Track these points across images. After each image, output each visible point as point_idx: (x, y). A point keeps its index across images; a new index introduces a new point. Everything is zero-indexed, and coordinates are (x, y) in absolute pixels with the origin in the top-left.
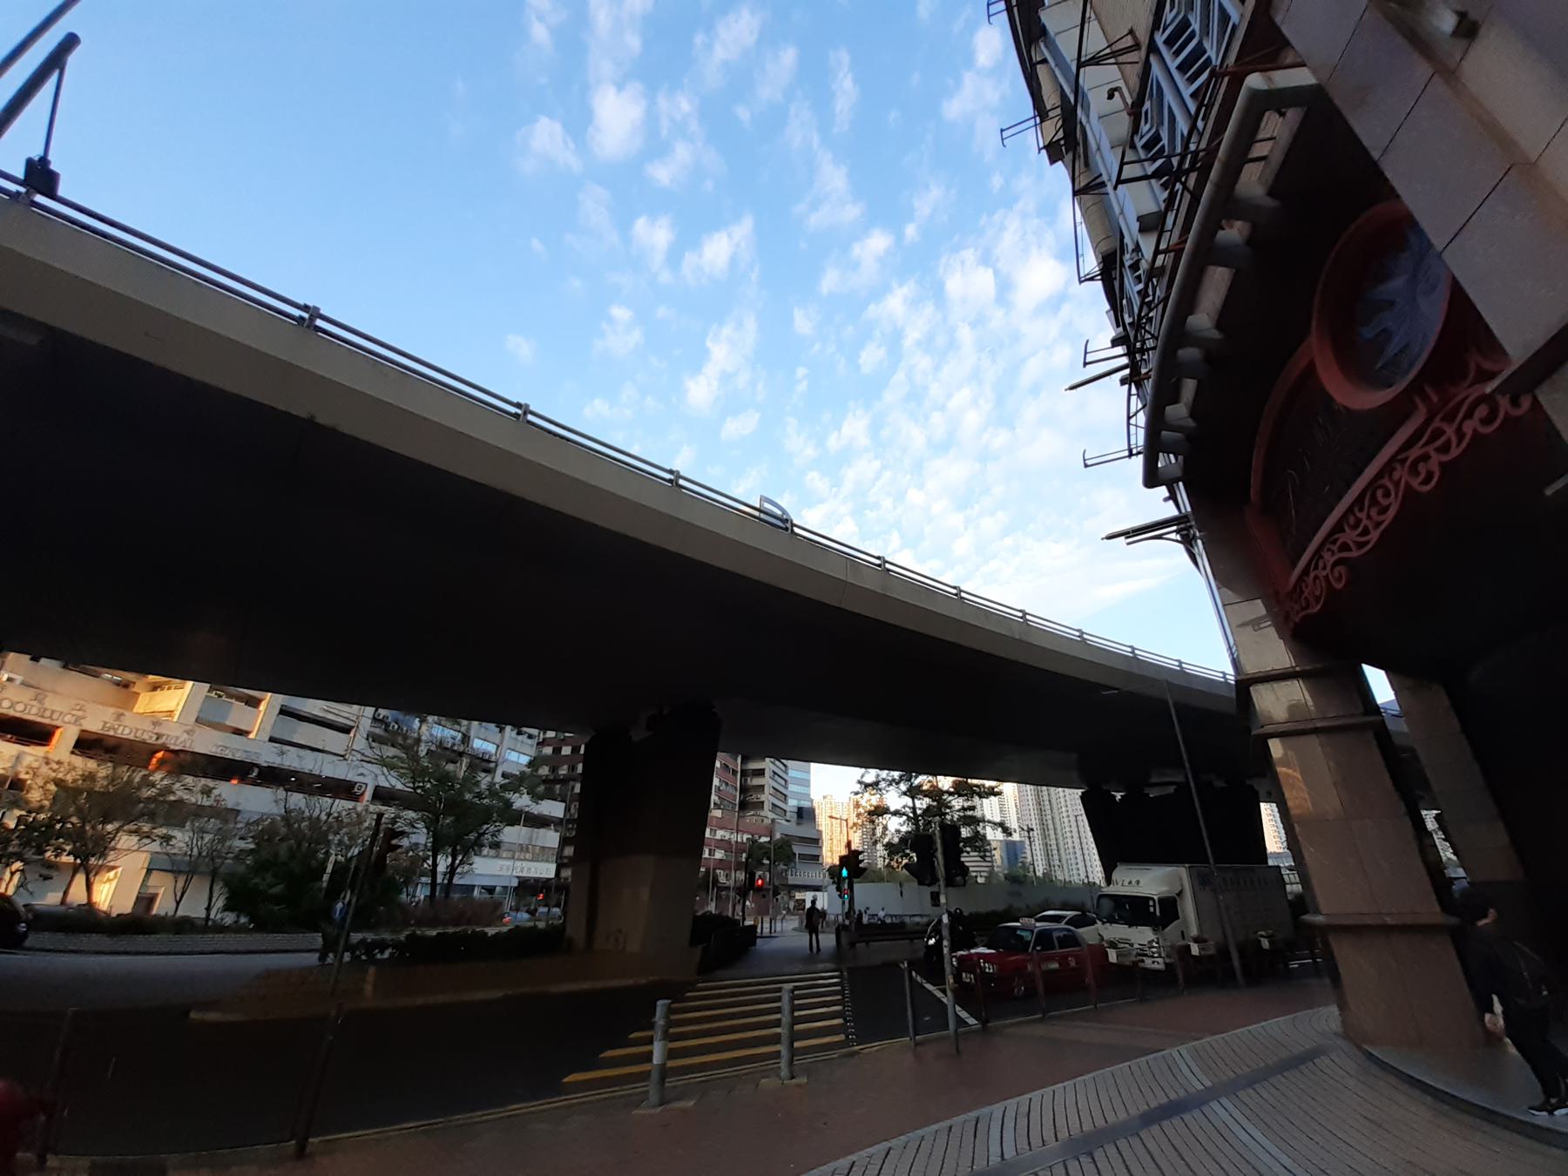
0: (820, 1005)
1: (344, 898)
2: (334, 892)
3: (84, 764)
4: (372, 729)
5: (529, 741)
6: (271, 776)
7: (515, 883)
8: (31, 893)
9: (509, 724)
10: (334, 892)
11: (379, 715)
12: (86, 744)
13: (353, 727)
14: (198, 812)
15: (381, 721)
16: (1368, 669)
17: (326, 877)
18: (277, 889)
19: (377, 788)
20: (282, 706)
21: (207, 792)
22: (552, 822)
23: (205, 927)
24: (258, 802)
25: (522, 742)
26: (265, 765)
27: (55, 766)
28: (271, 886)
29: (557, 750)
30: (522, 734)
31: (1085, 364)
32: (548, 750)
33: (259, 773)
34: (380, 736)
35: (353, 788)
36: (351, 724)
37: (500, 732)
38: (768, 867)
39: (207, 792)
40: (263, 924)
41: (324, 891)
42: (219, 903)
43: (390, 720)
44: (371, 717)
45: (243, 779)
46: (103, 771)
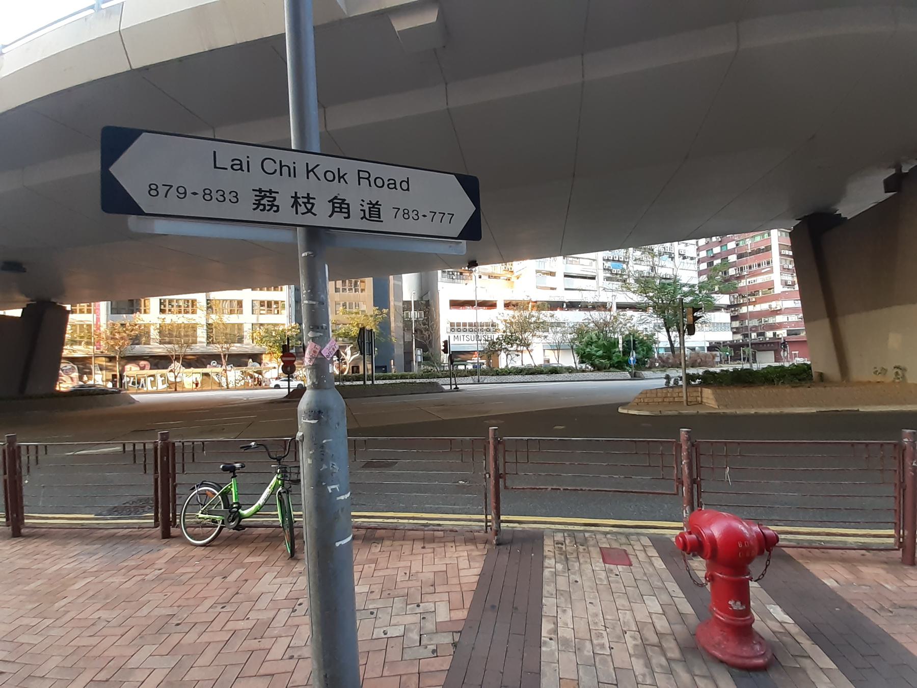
0: (292, 544)
1: (633, 355)
2: (626, 352)
3: (511, 312)
4: (605, 275)
5: (692, 262)
6: (572, 306)
7: (708, 345)
8: (515, 362)
9: (714, 236)
10: (626, 352)
11: (606, 267)
12: (507, 305)
13: (595, 276)
14: (552, 325)
15: (608, 269)
16: (349, 493)
17: (620, 346)
18: (600, 353)
19: (617, 304)
20: (564, 273)
21: (552, 316)
22: (722, 308)
23: (570, 370)
24: (576, 317)
25: (687, 263)
26: (567, 301)
27: (502, 315)
28: (597, 351)
29: (710, 264)
30: (686, 258)
31: (453, 215)
32: (704, 266)
33: (566, 305)
34: (609, 277)
35: (606, 305)
36: (595, 274)
37: (672, 260)
38: (666, 396)
39: (552, 316)
40: (598, 368)
41: (621, 352)
42: (577, 361)
43: (611, 268)
44: (602, 268)
45: (562, 308)
46: (517, 313)
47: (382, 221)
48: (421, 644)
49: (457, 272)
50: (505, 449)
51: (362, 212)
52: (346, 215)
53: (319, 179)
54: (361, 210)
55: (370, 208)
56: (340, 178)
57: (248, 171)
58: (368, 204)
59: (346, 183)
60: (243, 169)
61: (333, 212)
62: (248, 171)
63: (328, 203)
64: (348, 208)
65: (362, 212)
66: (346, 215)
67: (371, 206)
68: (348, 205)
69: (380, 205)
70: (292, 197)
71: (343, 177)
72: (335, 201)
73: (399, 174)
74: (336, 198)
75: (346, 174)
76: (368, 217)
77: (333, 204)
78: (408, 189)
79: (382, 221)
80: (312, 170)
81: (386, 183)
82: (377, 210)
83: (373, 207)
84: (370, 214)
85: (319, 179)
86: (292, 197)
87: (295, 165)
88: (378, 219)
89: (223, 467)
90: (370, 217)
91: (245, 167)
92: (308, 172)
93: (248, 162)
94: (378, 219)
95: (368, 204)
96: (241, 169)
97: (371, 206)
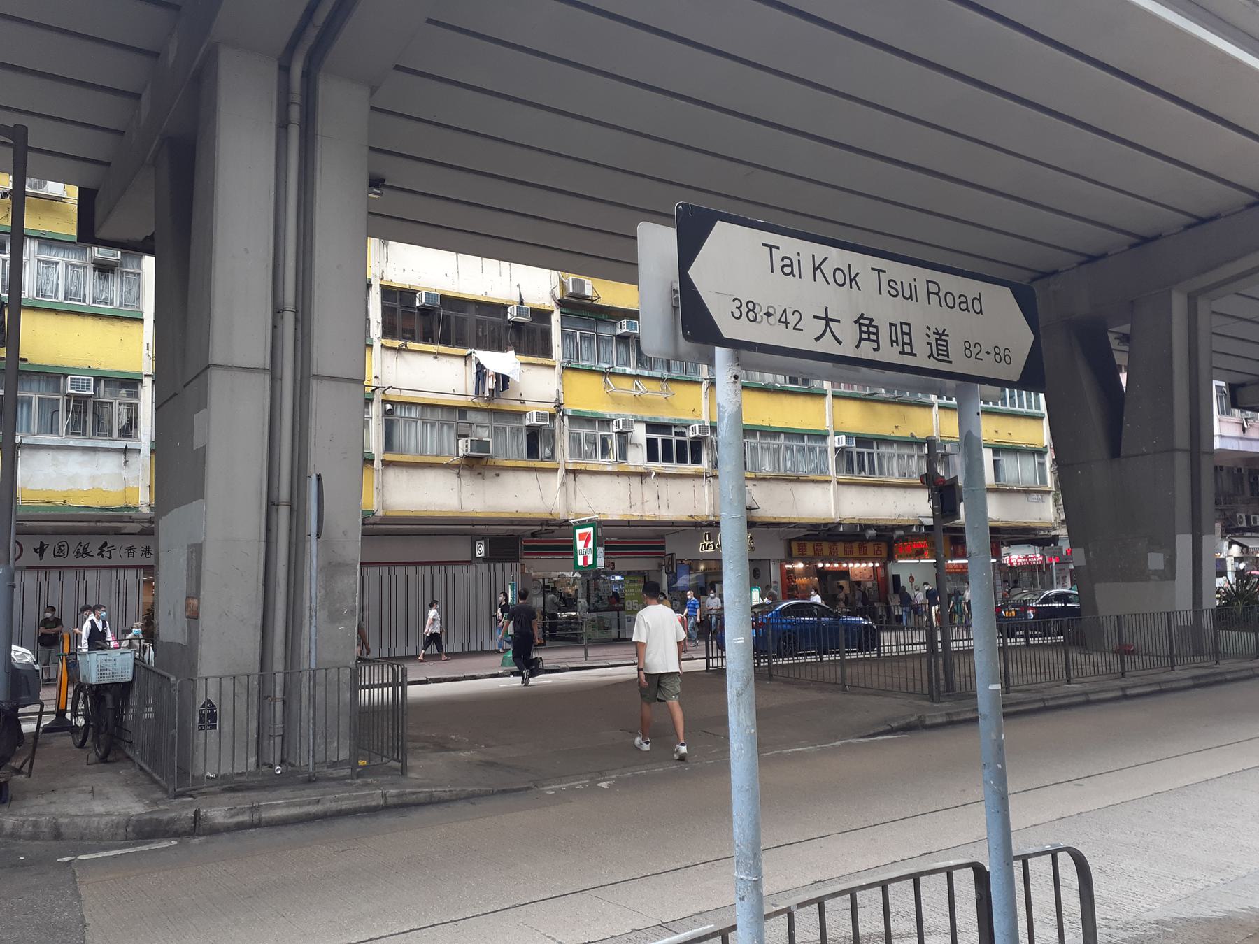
47: (951, 362)
48: (1213, 336)
49: (788, 677)
50: (1211, 362)
51: (929, 346)
52: (875, 345)
53: (828, 283)
54: (928, 343)
55: (937, 339)
56: (851, 280)
57: (800, 277)
58: (934, 333)
59: (859, 289)
60: (795, 273)
61: (861, 339)
62: (800, 277)
63: (841, 321)
64: (876, 334)
65: (929, 346)
66: (875, 345)
67: (938, 337)
68: (876, 327)
69: (947, 335)
70: (944, 330)
71: (819, 267)
72: (862, 321)
73: (971, 287)
74: (862, 316)
75: (858, 274)
76: (936, 356)
77: (861, 325)
78: (981, 312)
79: (951, 362)
80: (819, 267)
81: (958, 301)
82: (945, 343)
83: (940, 339)
84: (938, 350)
85: (828, 283)
86: (944, 330)
87: (799, 258)
88: (945, 358)
89: (993, 557)
90: (938, 354)
91: (796, 272)
92: (815, 270)
93: (799, 261)
94: (945, 358)
95: (934, 333)
96: (792, 273)
97: (938, 337)
